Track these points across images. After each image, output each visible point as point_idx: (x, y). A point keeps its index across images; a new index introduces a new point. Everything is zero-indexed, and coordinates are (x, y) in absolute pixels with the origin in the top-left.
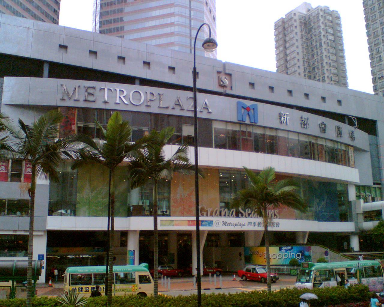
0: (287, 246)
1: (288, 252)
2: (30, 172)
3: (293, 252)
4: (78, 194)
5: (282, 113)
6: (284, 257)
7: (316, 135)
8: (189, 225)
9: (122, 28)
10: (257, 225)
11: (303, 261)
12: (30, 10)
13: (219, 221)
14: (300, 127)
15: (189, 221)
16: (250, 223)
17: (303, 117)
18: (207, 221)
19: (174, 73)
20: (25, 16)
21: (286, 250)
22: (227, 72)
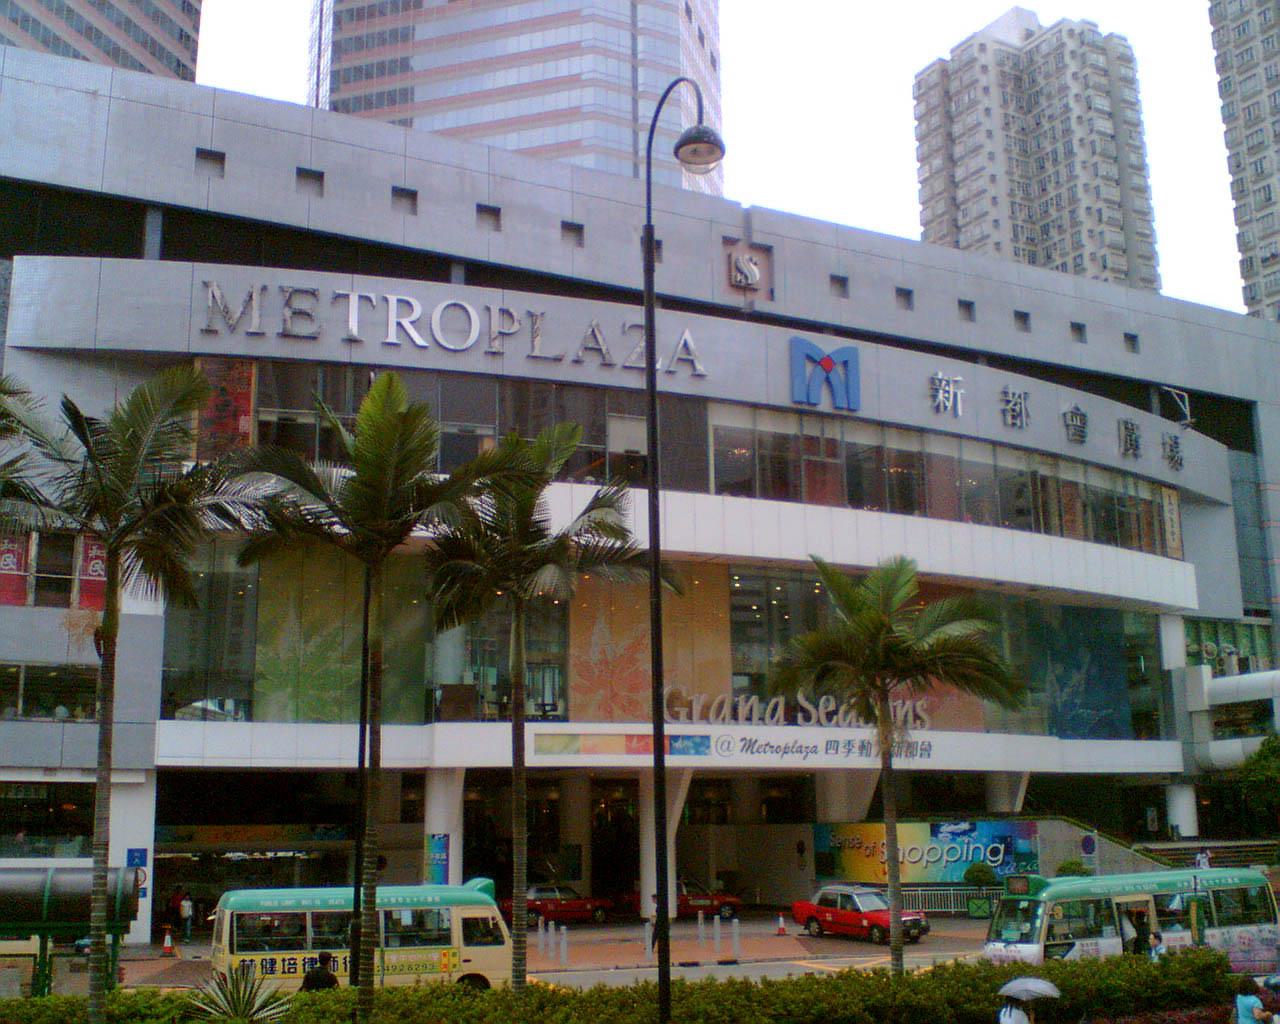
0: (957, 820)
1: (959, 839)
2: (99, 575)
3: (975, 841)
4: (259, 648)
5: (940, 376)
6: (945, 857)
7: (1054, 449)
8: (630, 751)
9: (406, 95)
10: (856, 750)
11: (1009, 871)
12: (99, 34)
13: (729, 739)
14: (1001, 423)
15: (629, 737)
16: (832, 745)
17: (1011, 391)
18: (688, 737)
19: (580, 243)
20: (83, 52)
21: (953, 833)
22: (758, 239)
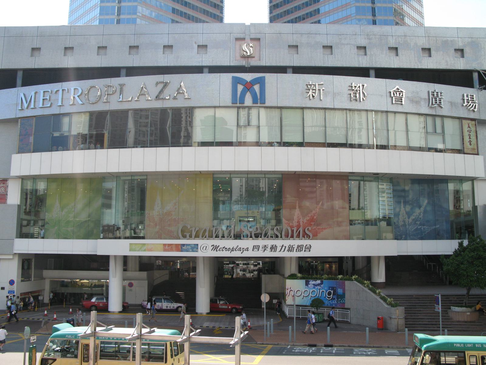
0: (316, 279)
1: (316, 287)
2: (3, 192)
3: (322, 288)
4: (47, 214)
5: (310, 83)
6: (311, 295)
7: (385, 109)
8: (165, 250)
9: (318, 11)
10: (269, 249)
11: (335, 302)
12: (208, 12)
13: (206, 245)
14: (390, 103)
15: (165, 245)
16: (256, 248)
17: (353, 85)
18: (189, 245)
19: (463, 56)
20: (208, 21)
21: (314, 285)
22: (253, 36)
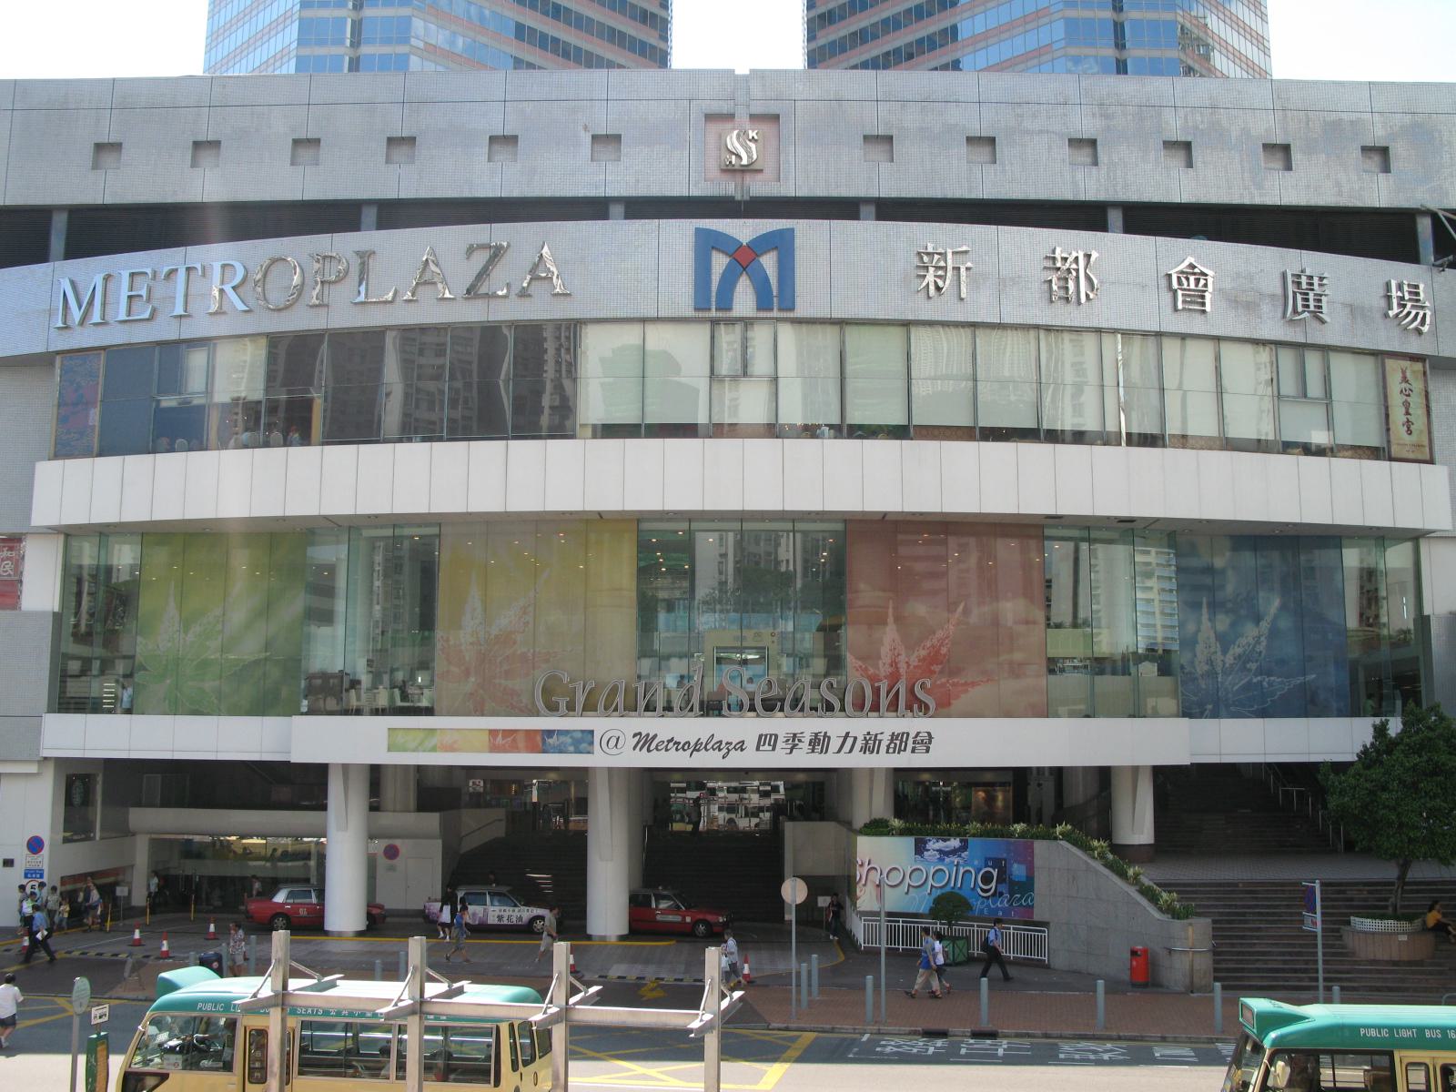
0: (946, 835)
1: (947, 860)
2: (9, 575)
3: (966, 863)
4: (139, 639)
5: (930, 250)
6: (930, 881)
7: (1153, 326)
8: (494, 749)
9: (951, 34)
10: (805, 746)
11: (1002, 903)
12: (622, 35)
13: (617, 734)
14: (1169, 309)
15: (493, 733)
16: (767, 741)
17: (1058, 255)
18: (566, 732)
20: (622, 61)
21: (940, 851)
22: (758, 108)
